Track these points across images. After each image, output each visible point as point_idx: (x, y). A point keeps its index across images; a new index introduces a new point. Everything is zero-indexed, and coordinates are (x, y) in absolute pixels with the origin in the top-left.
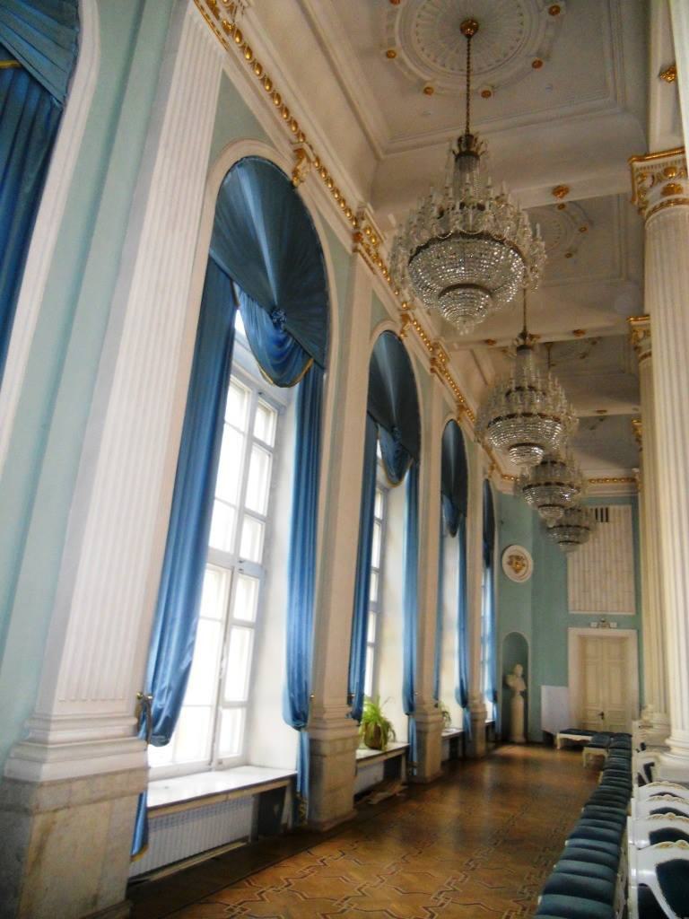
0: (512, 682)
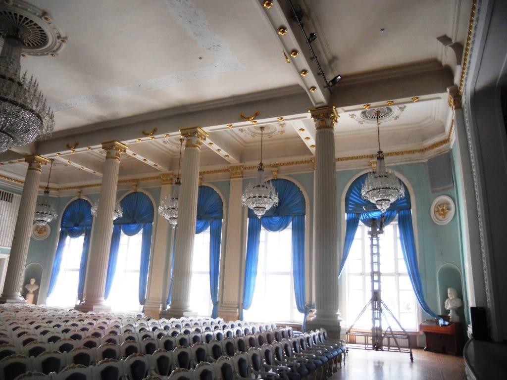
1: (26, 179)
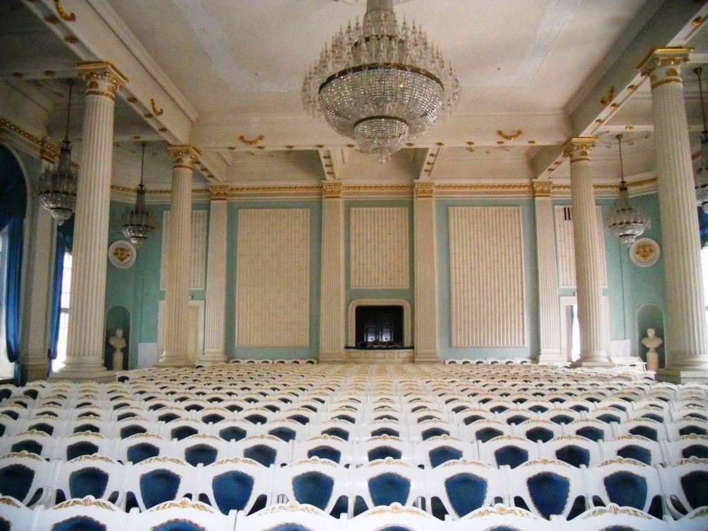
0: (113, 342)
1: (572, 180)
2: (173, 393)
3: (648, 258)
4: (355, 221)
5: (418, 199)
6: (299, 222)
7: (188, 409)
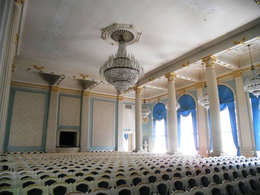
2: (55, 164)
3: (146, 121)
4: (62, 101)
5: (52, 92)
6: (41, 99)
7: (63, 168)
